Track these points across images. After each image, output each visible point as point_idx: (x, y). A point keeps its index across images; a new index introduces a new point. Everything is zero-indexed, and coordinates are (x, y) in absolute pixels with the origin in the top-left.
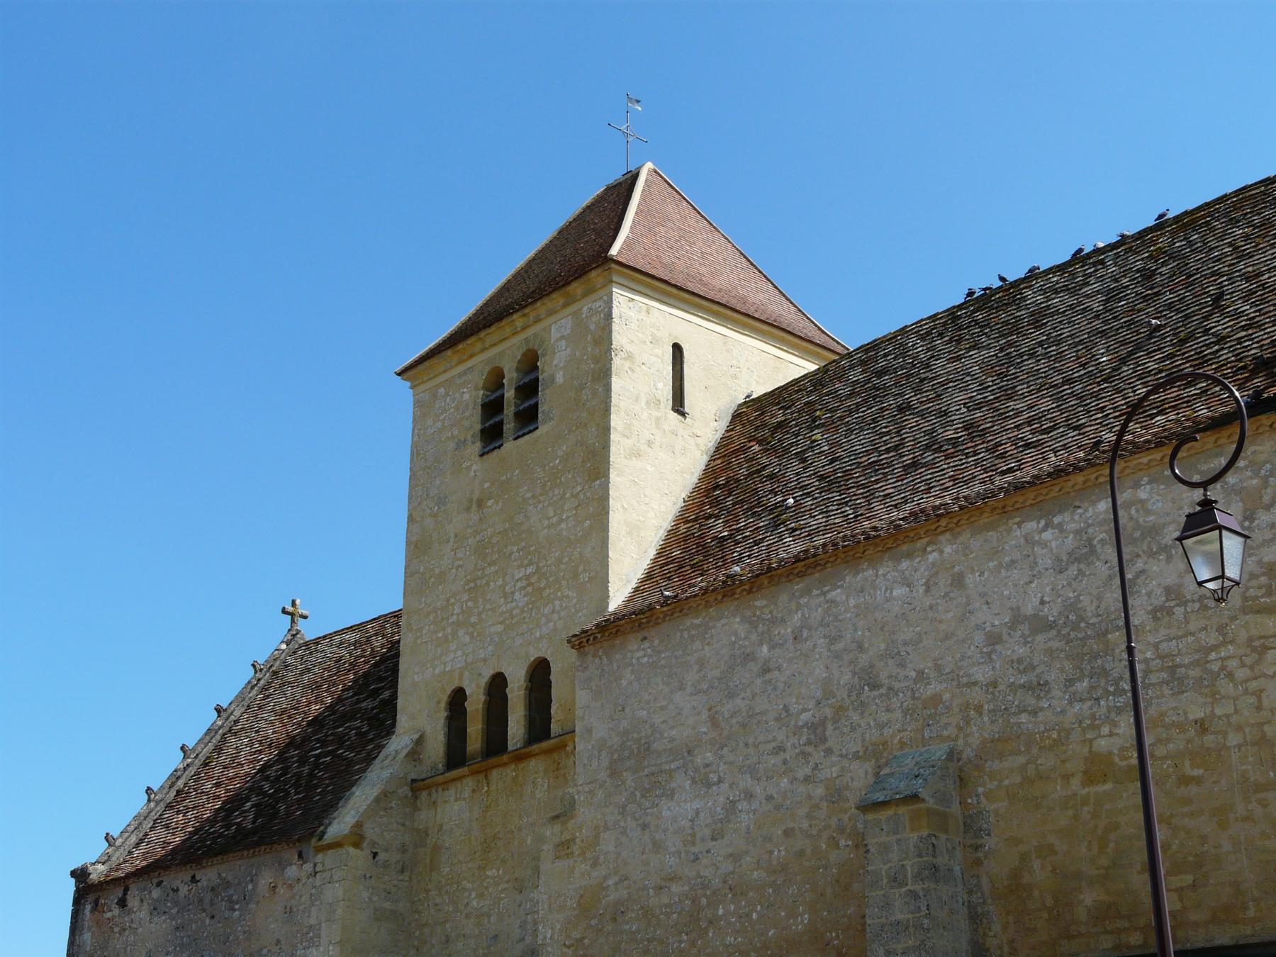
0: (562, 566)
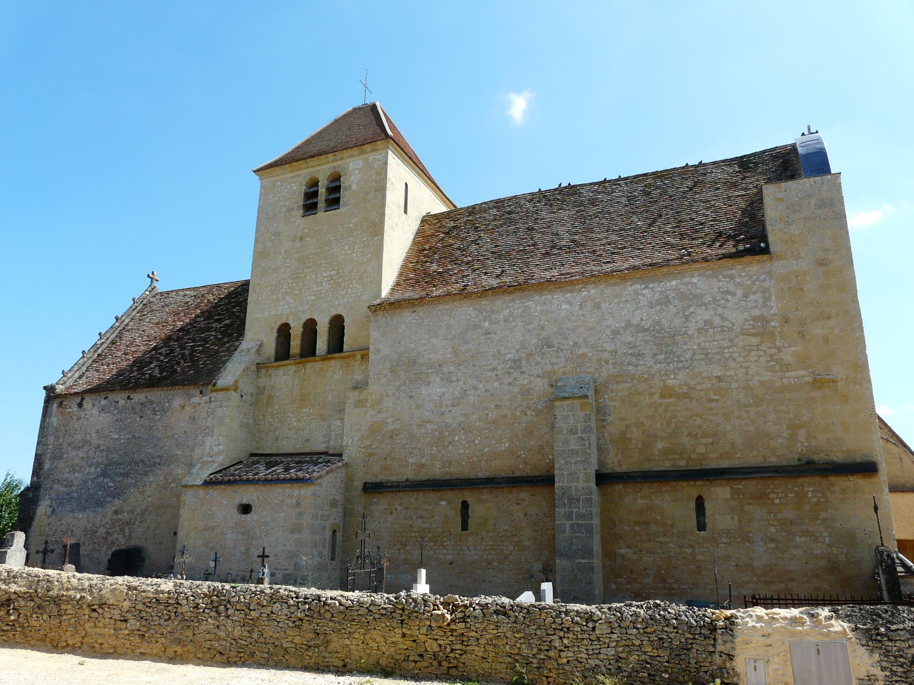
0: (353, 274)
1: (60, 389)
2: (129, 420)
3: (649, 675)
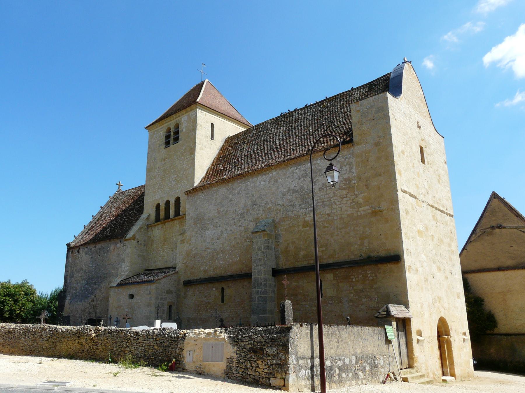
0: (184, 175)
1: (73, 244)
2: (95, 258)
3: (155, 358)
